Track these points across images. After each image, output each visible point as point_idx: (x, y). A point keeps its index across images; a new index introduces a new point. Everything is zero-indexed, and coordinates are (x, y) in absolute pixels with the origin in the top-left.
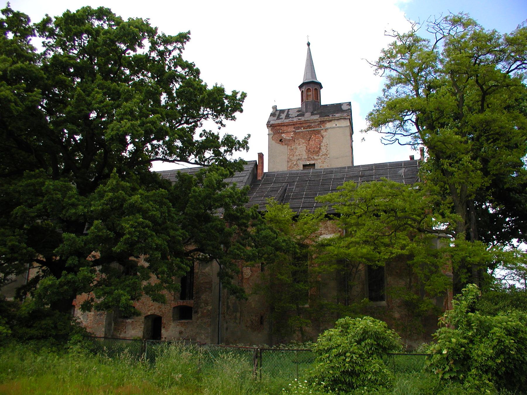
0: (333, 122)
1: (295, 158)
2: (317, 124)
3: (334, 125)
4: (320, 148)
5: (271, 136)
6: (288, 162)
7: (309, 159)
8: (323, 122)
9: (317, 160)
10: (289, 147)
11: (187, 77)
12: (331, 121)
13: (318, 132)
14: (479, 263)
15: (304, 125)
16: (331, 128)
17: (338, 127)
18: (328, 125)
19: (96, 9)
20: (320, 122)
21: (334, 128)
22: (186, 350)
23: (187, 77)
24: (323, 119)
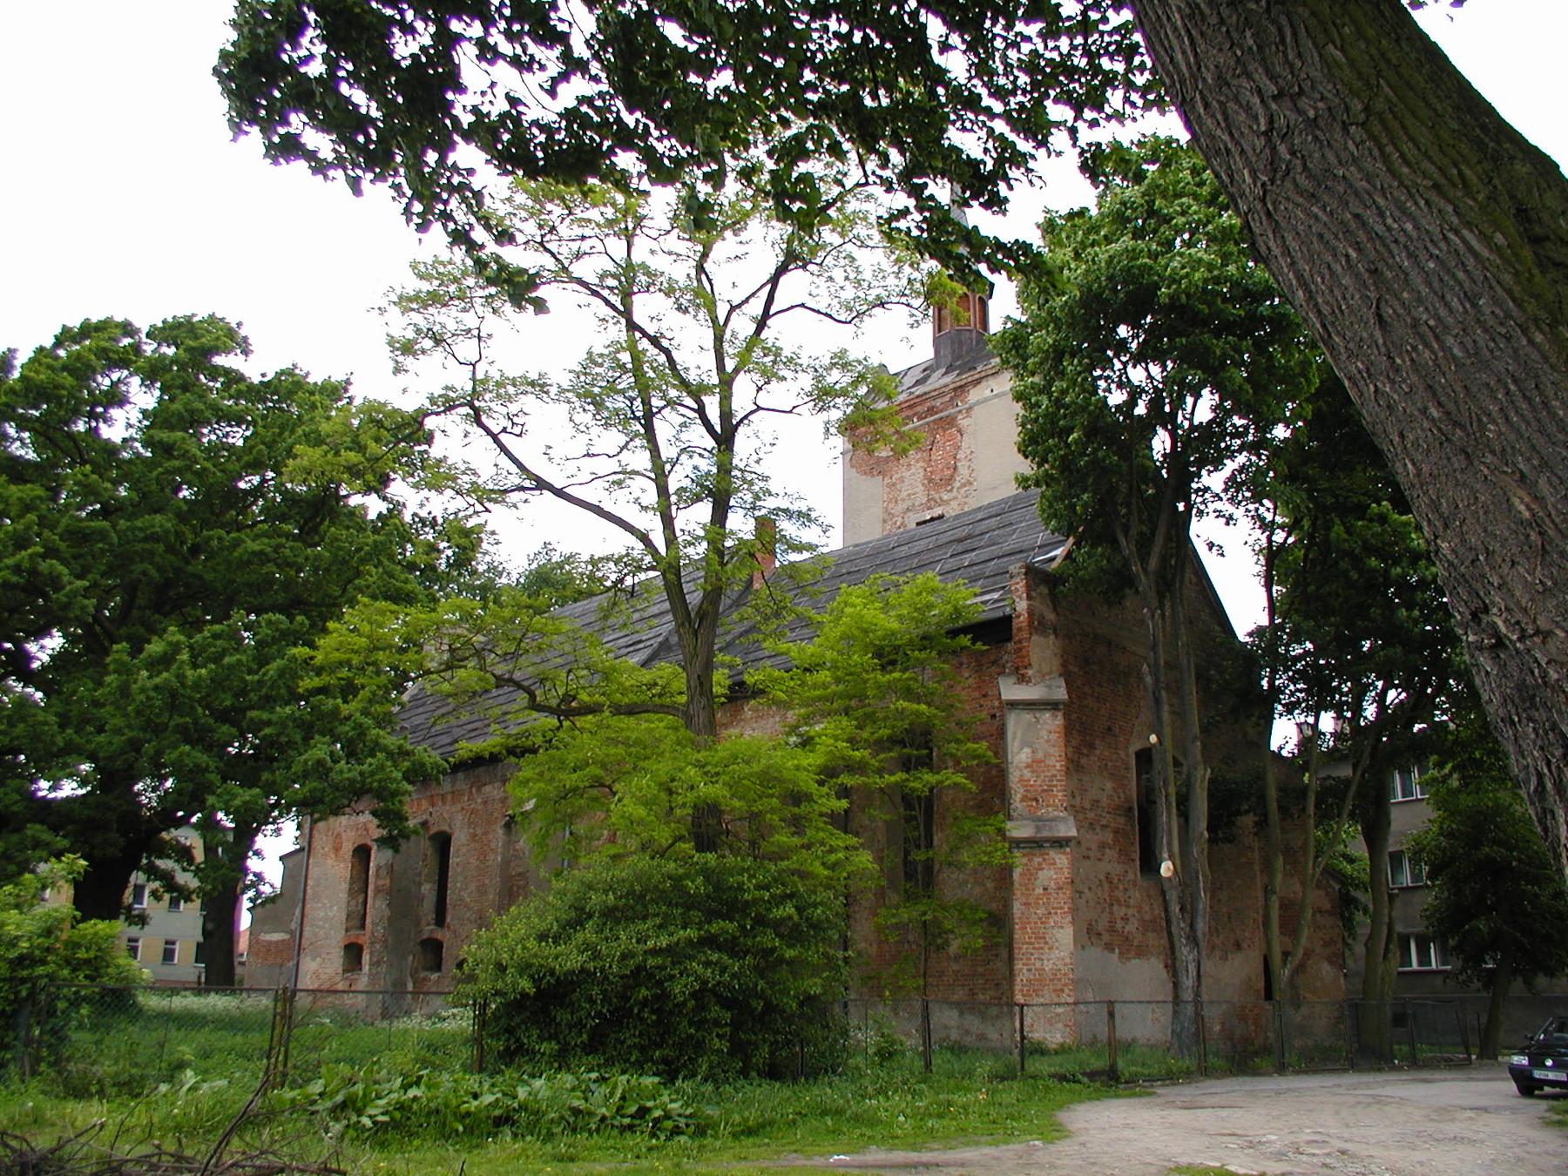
0: (984, 384)
1: (901, 507)
2: (947, 398)
3: (988, 393)
4: (955, 468)
5: (848, 456)
6: (885, 521)
7: (931, 503)
8: (961, 390)
9: (947, 502)
10: (887, 480)
11: (62, 353)
12: (978, 382)
13: (950, 422)
14: (1062, 1045)
15: (919, 409)
16: (978, 403)
17: (996, 396)
18: (974, 395)
19: (227, 102)
20: (955, 389)
21: (986, 400)
22: (1456, 336)
23: (62, 353)
24: (967, 377)
